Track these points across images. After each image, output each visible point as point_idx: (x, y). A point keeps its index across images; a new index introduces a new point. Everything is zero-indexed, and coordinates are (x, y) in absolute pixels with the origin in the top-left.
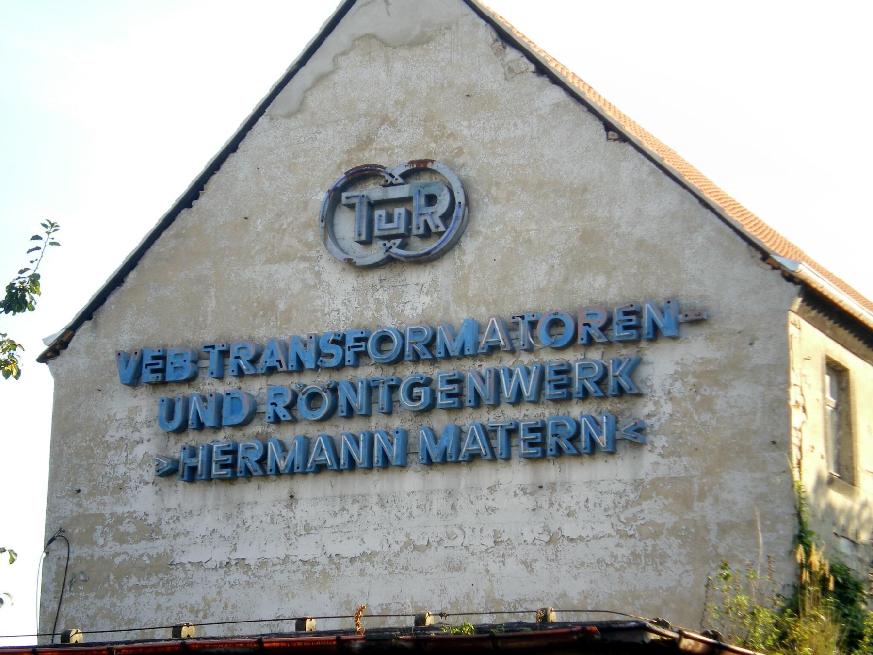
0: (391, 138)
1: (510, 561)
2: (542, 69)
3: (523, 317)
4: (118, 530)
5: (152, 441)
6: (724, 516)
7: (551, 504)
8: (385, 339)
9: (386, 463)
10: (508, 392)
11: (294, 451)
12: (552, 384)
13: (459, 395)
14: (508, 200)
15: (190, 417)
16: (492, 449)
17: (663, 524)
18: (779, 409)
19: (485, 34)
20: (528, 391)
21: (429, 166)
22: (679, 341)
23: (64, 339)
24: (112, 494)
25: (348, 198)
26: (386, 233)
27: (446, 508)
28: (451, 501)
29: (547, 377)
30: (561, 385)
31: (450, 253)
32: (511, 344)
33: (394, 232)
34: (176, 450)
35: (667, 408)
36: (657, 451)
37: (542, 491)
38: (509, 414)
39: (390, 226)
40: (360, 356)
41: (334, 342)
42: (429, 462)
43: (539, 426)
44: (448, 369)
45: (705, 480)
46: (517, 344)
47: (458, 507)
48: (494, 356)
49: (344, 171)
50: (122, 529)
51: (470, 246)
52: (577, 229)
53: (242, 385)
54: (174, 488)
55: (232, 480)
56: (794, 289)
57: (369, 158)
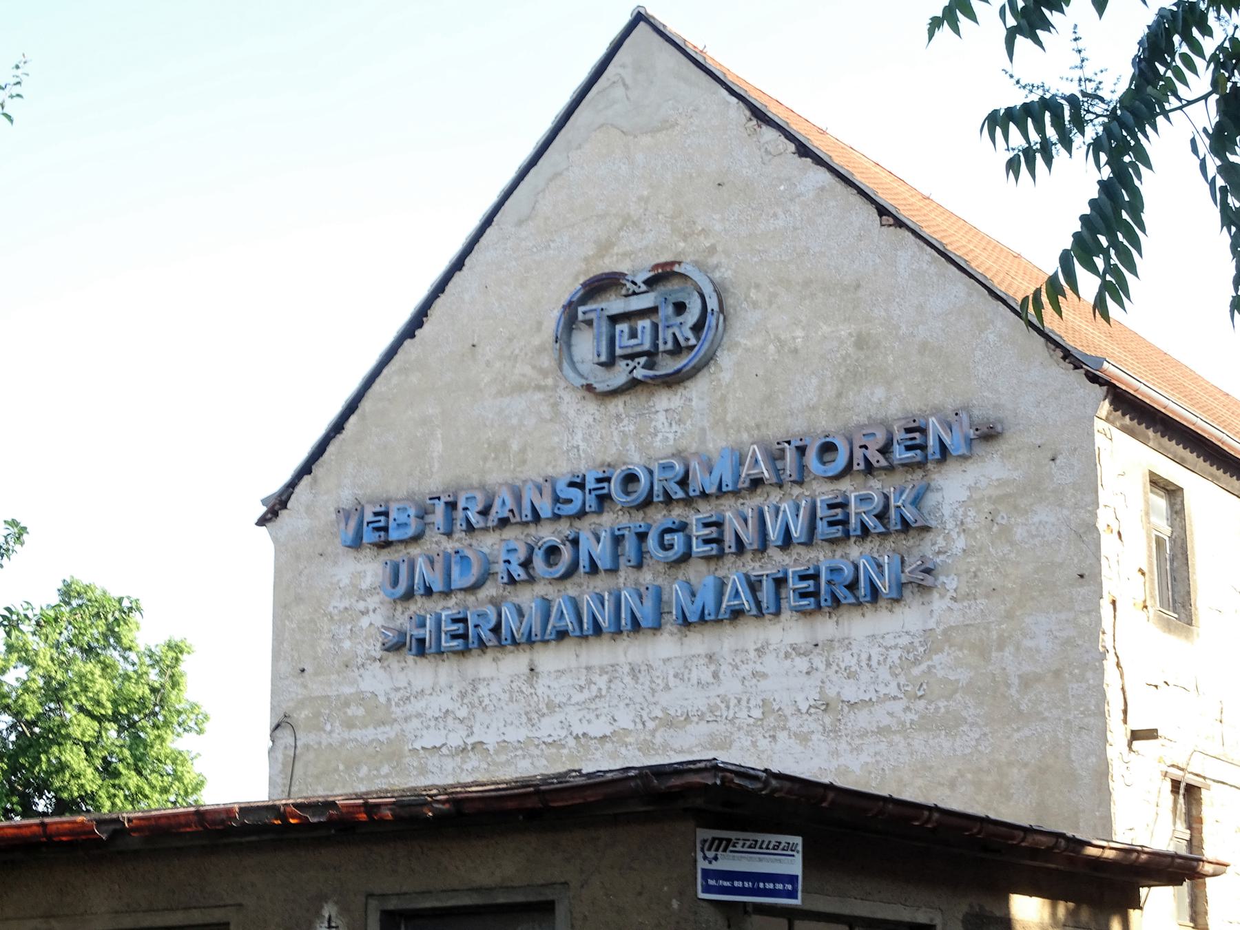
0: (633, 239)
1: (782, 735)
2: (803, 150)
3: (789, 443)
4: (345, 713)
5: (378, 611)
6: (1027, 668)
7: (828, 665)
8: (630, 478)
9: (636, 626)
10: (774, 534)
11: (531, 615)
12: (825, 521)
13: (719, 541)
14: (770, 303)
15: (416, 581)
16: (758, 604)
17: (957, 681)
18: (1086, 534)
19: (738, 112)
20: (797, 533)
21: (676, 268)
22: (971, 461)
23: (284, 498)
24: (338, 673)
25: (584, 313)
26: (629, 351)
27: (707, 676)
28: (713, 667)
29: (819, 514)
30: (840, 525)
31: (705, 371)
32: (778, 476)
33: (639, 349)
34: (402, 620)
35: (960, 543)
36: (949, 595)
37: (818, 650)
38: (778, 562)
39: (633, 342)
40: (604, 500)
41: (572, 484)
42: (686, 623)
43: (811, 572)
44: (706, 511)
45: (1004, 626)
46: (785, 477)
47: (721, 675)
48: (759, 491)
49: (581, 281)
50: (350, 712)
51: (725, 359)
52: (850, 334)
53: (474, 543)
54: (403, 664)
55: (464, 652)
56: (1101, 391)
57: (608, 265)
